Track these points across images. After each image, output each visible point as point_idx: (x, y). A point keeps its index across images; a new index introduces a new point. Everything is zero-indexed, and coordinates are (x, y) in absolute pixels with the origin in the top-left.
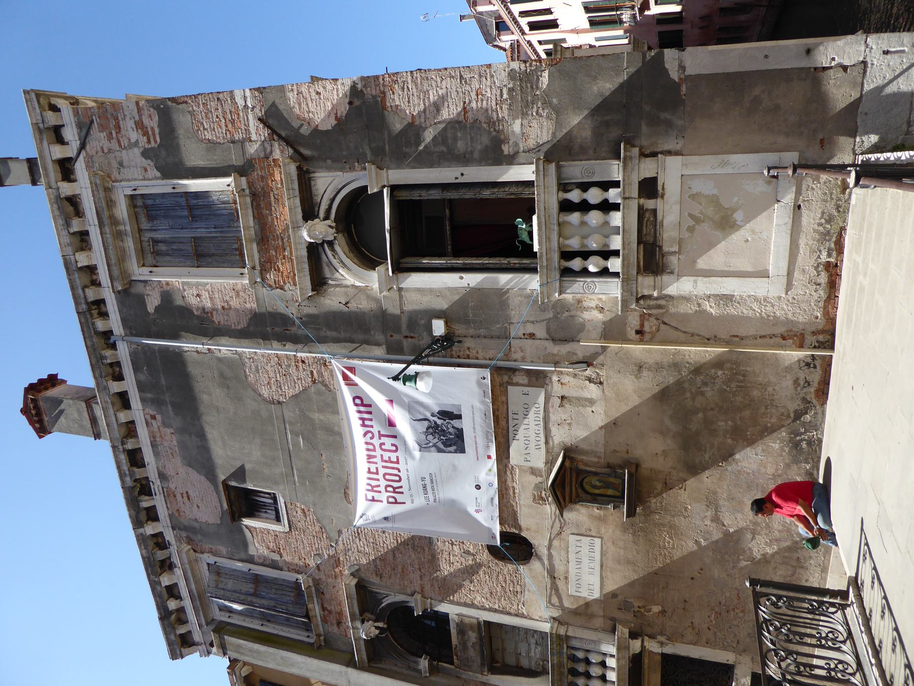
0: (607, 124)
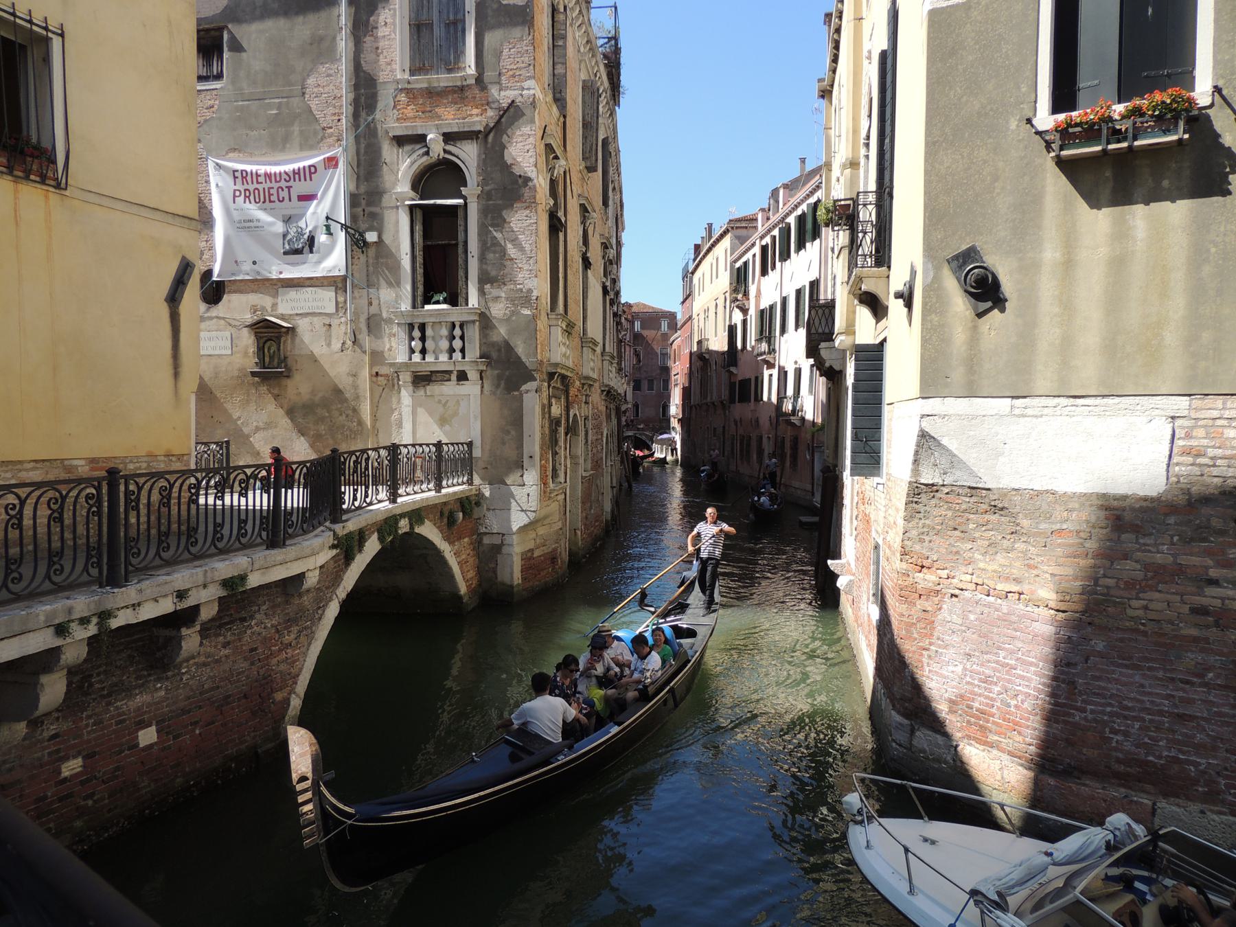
0: (499, 350)
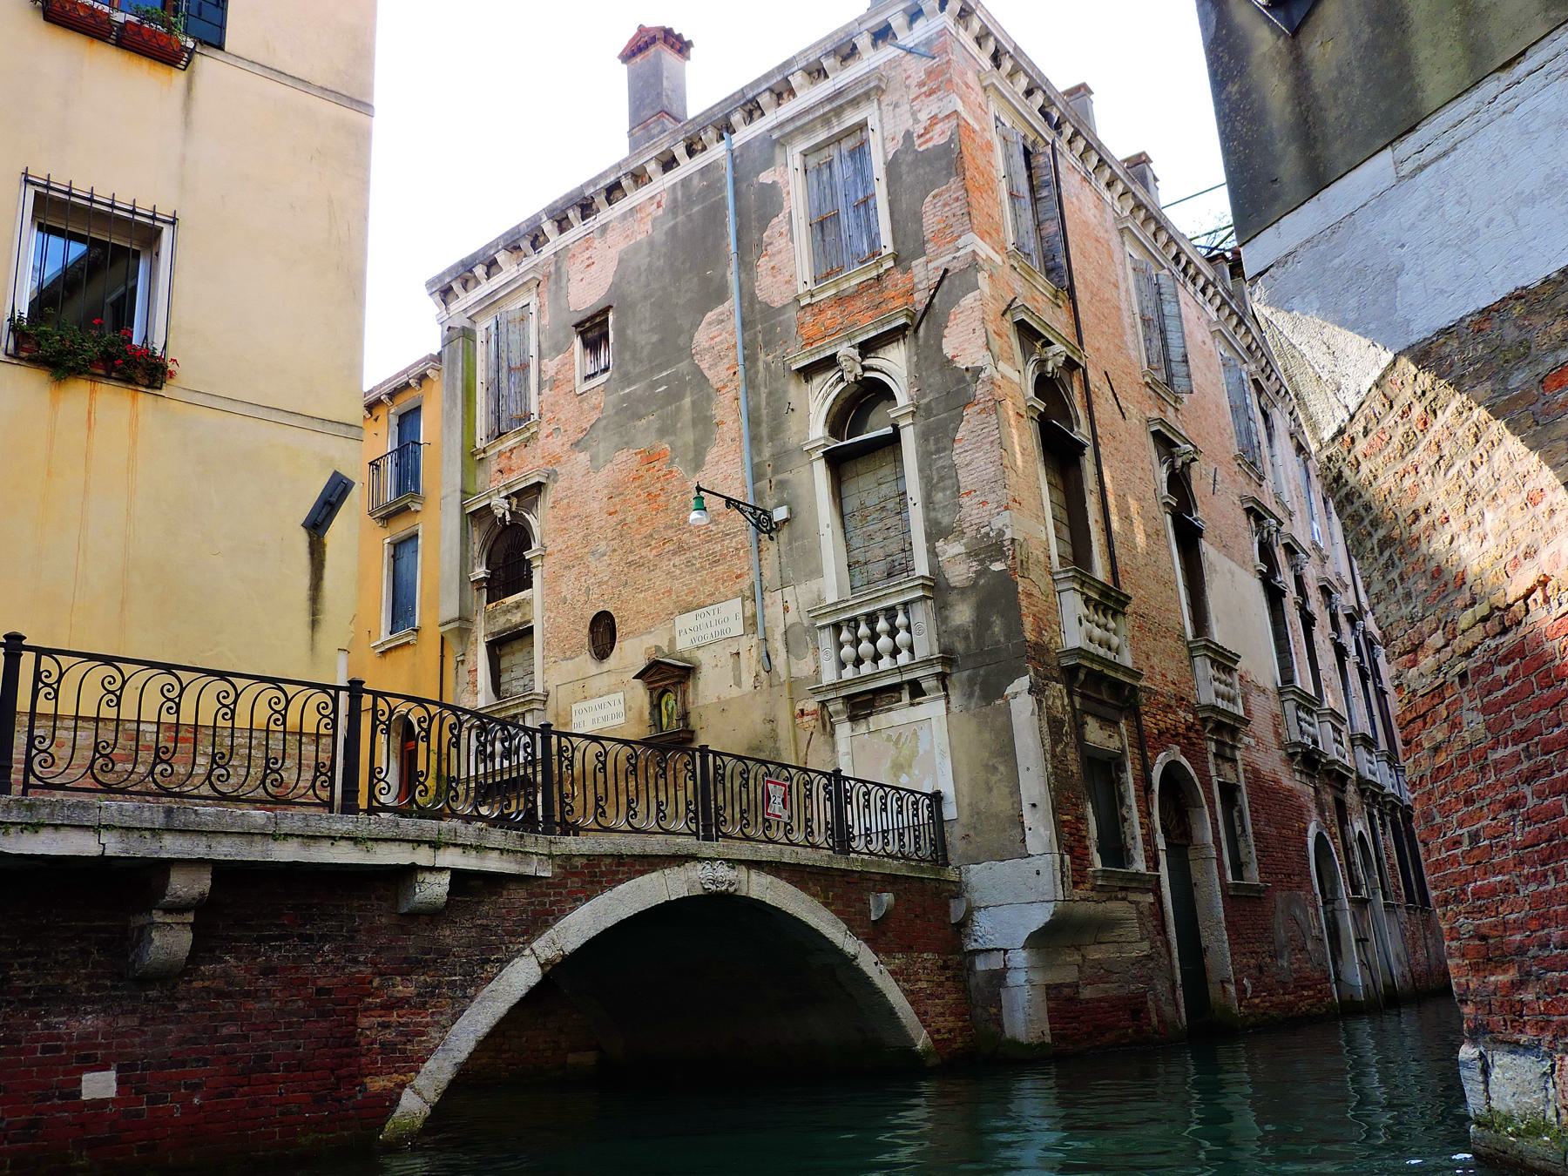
0: (967, 638)
